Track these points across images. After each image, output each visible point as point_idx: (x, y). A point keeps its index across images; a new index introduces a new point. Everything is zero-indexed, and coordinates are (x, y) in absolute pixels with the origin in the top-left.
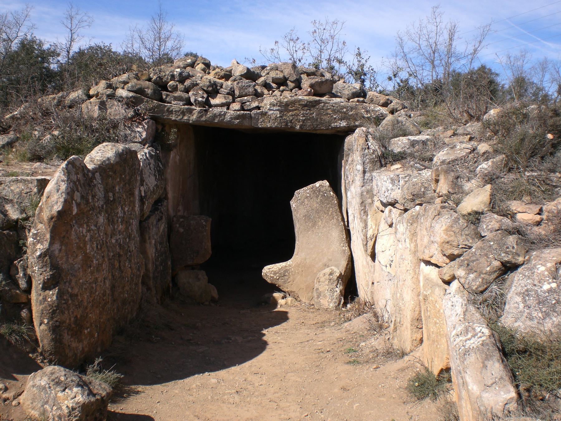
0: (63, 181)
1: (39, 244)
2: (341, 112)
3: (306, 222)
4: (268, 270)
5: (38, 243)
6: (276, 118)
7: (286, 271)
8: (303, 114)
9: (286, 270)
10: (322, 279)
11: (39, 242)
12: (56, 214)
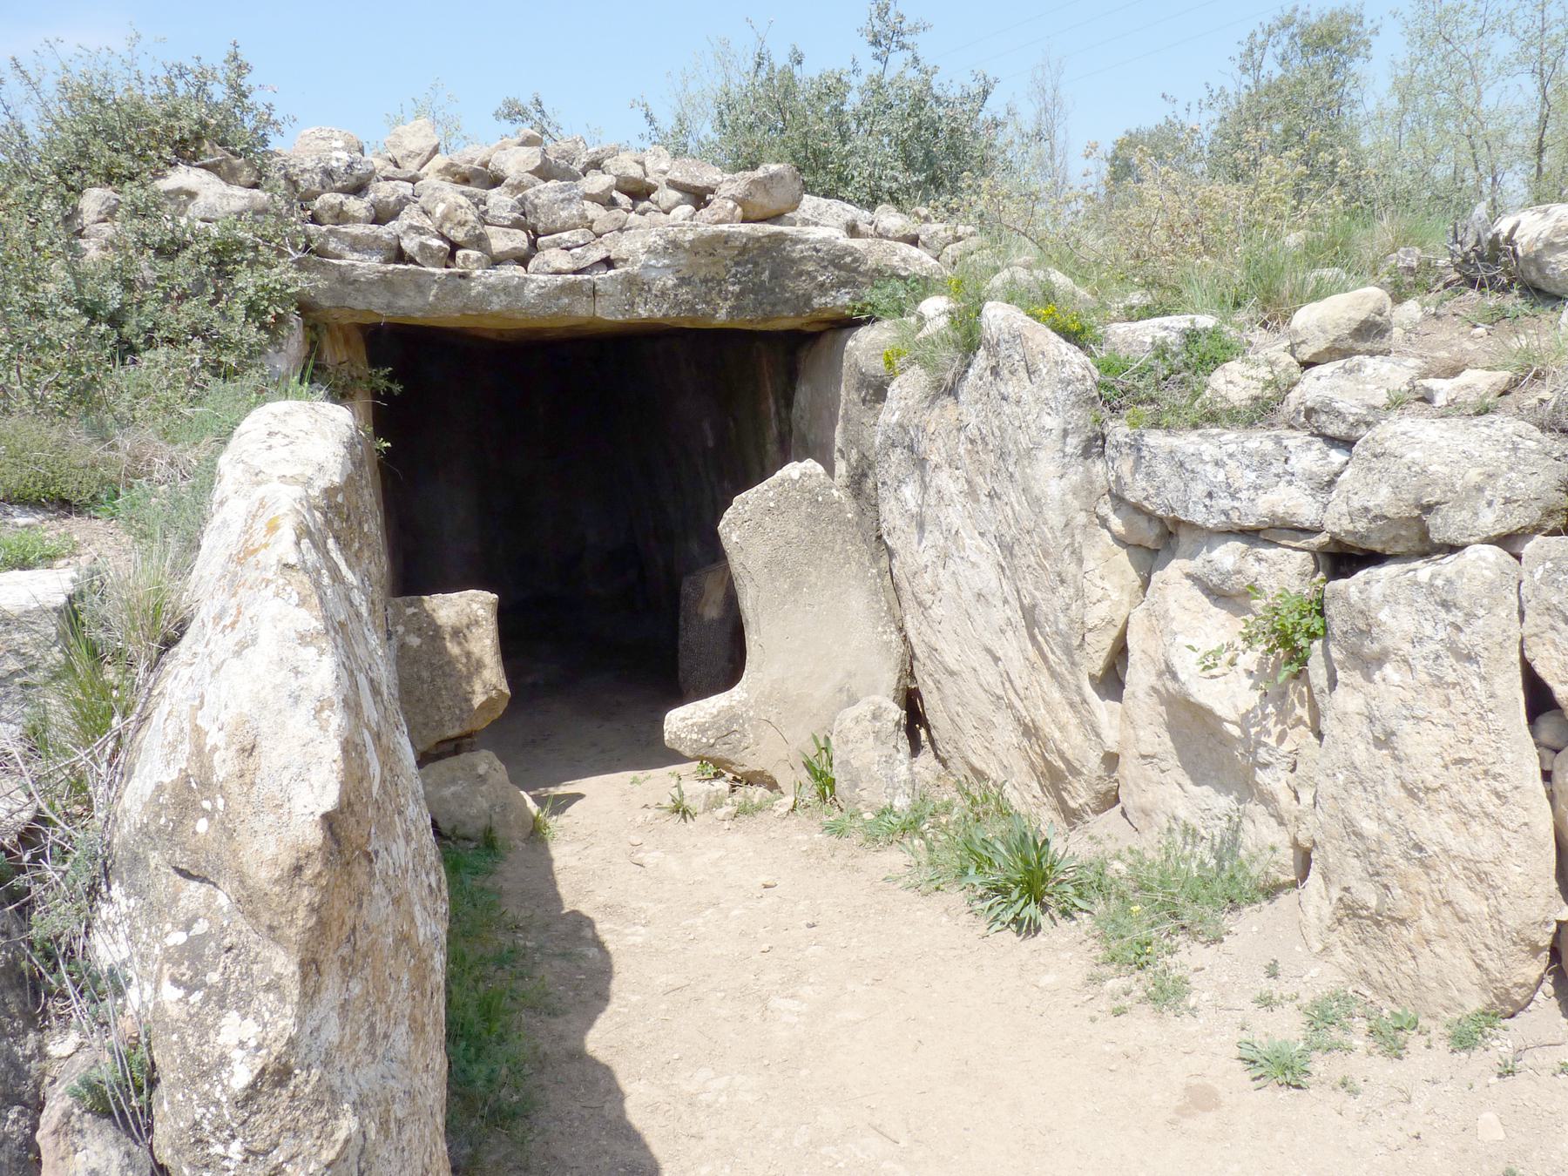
0: (304, 639)
1: (233, 1016)
2: (837, 266)
3: (773, 580)
4: (681, 725)
5: (222, 1005)
6: (663, 293)
7: (733, 718)
8: (735, 276)
9: (732, 717)
10: (856, 733)
11: (220, 998)
12: (314, 836)
